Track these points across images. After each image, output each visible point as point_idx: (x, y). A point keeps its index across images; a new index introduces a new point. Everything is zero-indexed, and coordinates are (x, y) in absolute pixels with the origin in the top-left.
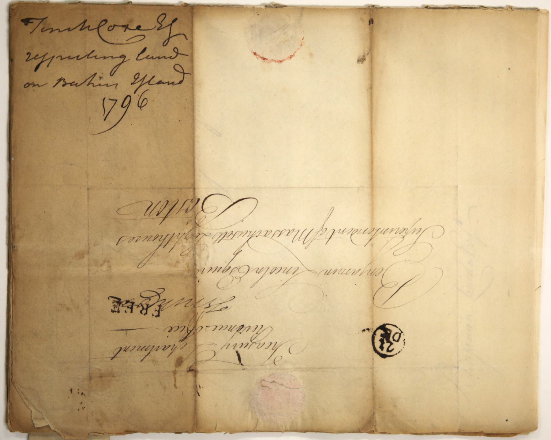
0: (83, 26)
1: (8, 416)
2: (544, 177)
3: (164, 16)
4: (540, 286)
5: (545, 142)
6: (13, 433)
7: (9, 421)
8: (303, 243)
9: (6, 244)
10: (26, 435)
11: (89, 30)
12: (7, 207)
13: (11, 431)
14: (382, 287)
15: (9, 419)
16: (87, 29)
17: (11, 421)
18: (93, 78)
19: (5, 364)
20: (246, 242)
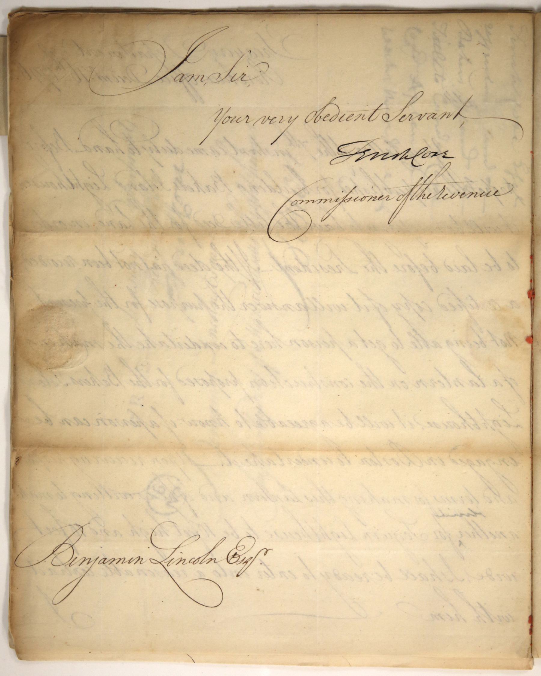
0: (375, 199)
1: (29, 12)
2: (328, 665)
3: (449, 164)
4: (194, 662)
5: (372, 665)
6: (7, 16)
7: (23, 13)
8: (99, 562)
9: (239, 8)
10: (5, 33)
11: (372, 196)
12: (289, 7)
13: (10, 15)
14: (448, 172)
15: (27, 14)
16: (373, 197)
17: (24, 16)
18: (207, 556)
19: (92, 7)
20: (236, 338)
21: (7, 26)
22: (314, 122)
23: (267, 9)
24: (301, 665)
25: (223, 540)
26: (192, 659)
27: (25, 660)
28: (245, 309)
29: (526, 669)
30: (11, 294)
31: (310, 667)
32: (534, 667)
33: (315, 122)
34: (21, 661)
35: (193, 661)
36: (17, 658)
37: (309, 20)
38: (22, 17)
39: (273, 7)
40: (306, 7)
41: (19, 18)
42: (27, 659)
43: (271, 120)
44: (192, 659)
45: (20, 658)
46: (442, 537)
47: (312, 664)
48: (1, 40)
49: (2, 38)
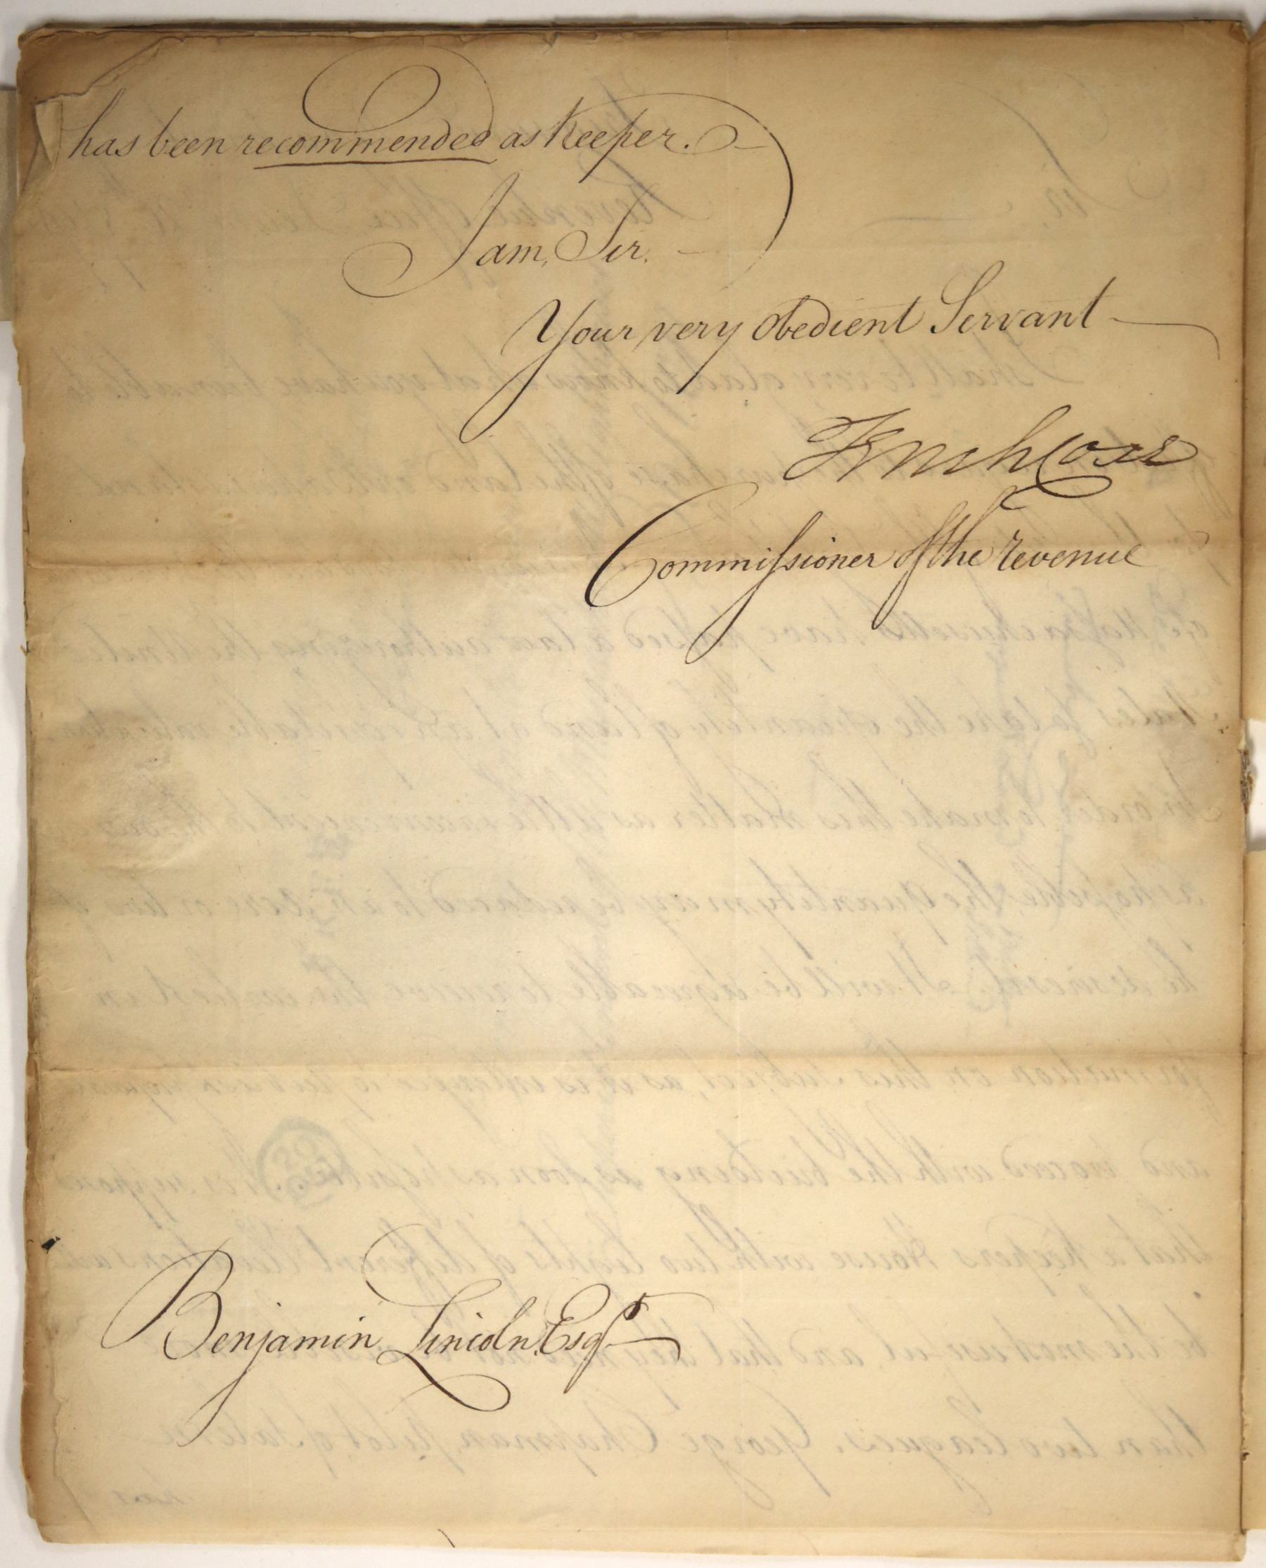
1: (65, 29)
2: (764, 1553)
4: (454, 1546)
9: (557, 19)
10: (12, 80)
13: (22, 39)
15: (59, 32)
17: (53, 37)
19: (213, 20)
21: (15, 67)
22: (632, 257)
23: (623, 21)
24: (701, 1553)
25: (572, 1382)
26: (449, 1539)
27: (55, 1542)
28: (1046, 1264)
29: (1228, 1560)
30: (31, 944)
31: (723, 1556)
32: (1247, 1558)
33: (634, 257)
34: (49, 1544)
35: (451, 1543)
36: (40, 1537)
37: (719, 46)
38: (49, 38)
39: (635, 18)
40: (718, 18)
41: (40, 41)
42: (62, 1539)
43: (794, 332)
44: (449, 1539)
45: (47, 1538)
46: (797, 990)
47: (726, 1550)
48: (2, 97)
49: (5, 93)
